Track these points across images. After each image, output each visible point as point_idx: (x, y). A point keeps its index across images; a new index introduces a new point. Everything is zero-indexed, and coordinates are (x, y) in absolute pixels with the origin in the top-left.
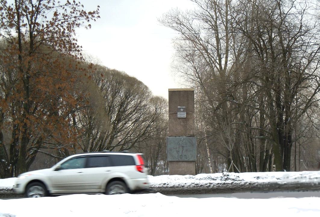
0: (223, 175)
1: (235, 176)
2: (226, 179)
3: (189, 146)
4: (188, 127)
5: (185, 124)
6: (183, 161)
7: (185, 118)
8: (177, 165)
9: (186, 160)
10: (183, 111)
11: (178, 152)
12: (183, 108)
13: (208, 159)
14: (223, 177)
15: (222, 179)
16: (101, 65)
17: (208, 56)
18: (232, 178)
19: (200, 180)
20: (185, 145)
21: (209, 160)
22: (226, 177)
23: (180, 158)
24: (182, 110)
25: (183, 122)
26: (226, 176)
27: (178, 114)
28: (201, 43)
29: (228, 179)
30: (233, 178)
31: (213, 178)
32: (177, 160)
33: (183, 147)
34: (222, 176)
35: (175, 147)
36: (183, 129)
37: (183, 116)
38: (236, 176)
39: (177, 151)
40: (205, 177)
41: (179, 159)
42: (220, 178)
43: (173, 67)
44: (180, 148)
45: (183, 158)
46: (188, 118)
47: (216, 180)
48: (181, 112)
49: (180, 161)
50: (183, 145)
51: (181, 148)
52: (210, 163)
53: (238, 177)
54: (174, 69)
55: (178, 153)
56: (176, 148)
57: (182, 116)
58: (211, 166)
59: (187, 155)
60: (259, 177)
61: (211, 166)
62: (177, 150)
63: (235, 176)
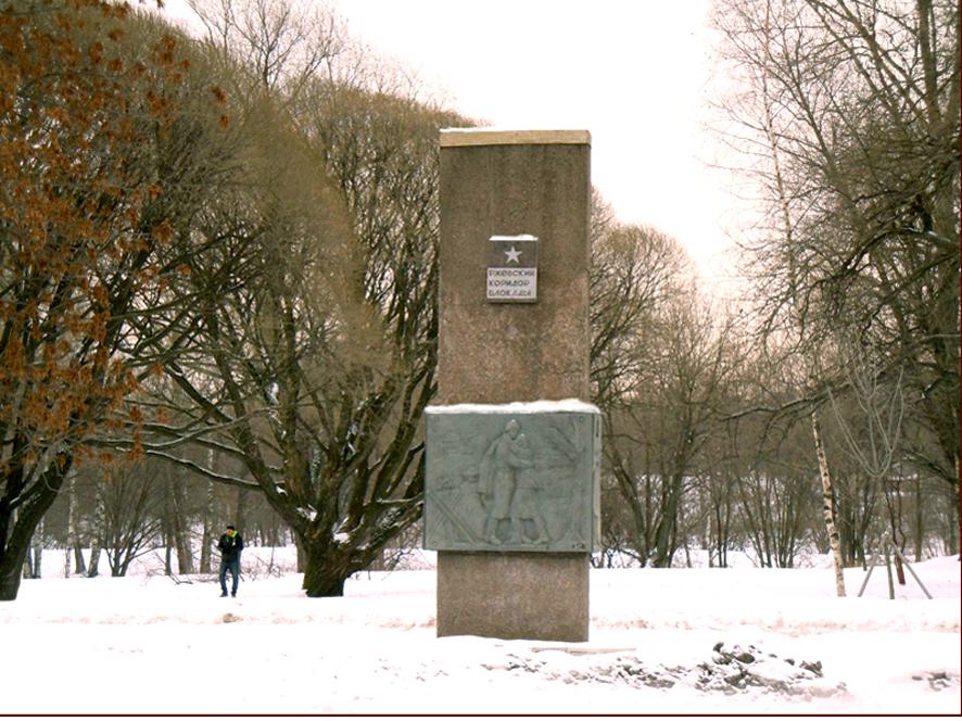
0: (717, 656)
1: (791, 662)
2: (734, 681)
3: (551, 467)
4: (547, 357)
5: (534, 335)
6: (512, 555)
7: (531, 304)
8: (478, 577)
9: (528, 546)
10: (522, 264)
11: (485, 498)
12: (517, 245)
13: (823, 502)
14: (715, 667)
15: (705, 681)
16: (421, 99)
17: (879, 63)
18: (769, 677)
19: (568, 682)
20: (526, 462)
21: (827, 508)
22: (732, 670)
23: (498, 537)
24: (513, 255)
25: (522, 327)
26: (734, 663)
27: (490, 278)
28: (848, 12)
29: (749, 682)
30: (779, 678)
31: (650, 669)
32: (481, 546)
33: (515, 470)
34: (710, 663)
35: (469, 473)
36: (516, 366)
37: (519, 289)
38: (797, 663)
39: (480, 494)
40: (606, 667)
41: (490, 542)
42: (695, 676)
43: (711, 104)
44: (500, 474)
45: (515, 536)
46: (548, 300)
47: (671, 684)
48: (505, 266)
49: (497, 554)
50: (514, 460)
51: (504, 478)
52: (829, 521)
53: (816, 668)
54: (714, 109)
55: (487, 503)
56: (477, 477)
57: (515, 293)
58: (835, 535)
59: (537, 520)
60: (943, 676)
61: (835, 535)
62: (482, 485)
63: (791, 662)
